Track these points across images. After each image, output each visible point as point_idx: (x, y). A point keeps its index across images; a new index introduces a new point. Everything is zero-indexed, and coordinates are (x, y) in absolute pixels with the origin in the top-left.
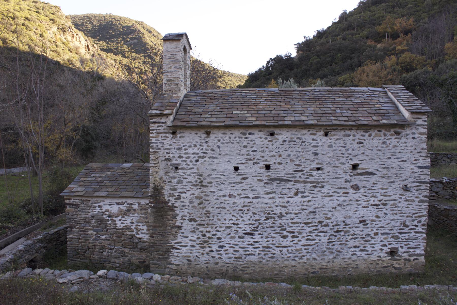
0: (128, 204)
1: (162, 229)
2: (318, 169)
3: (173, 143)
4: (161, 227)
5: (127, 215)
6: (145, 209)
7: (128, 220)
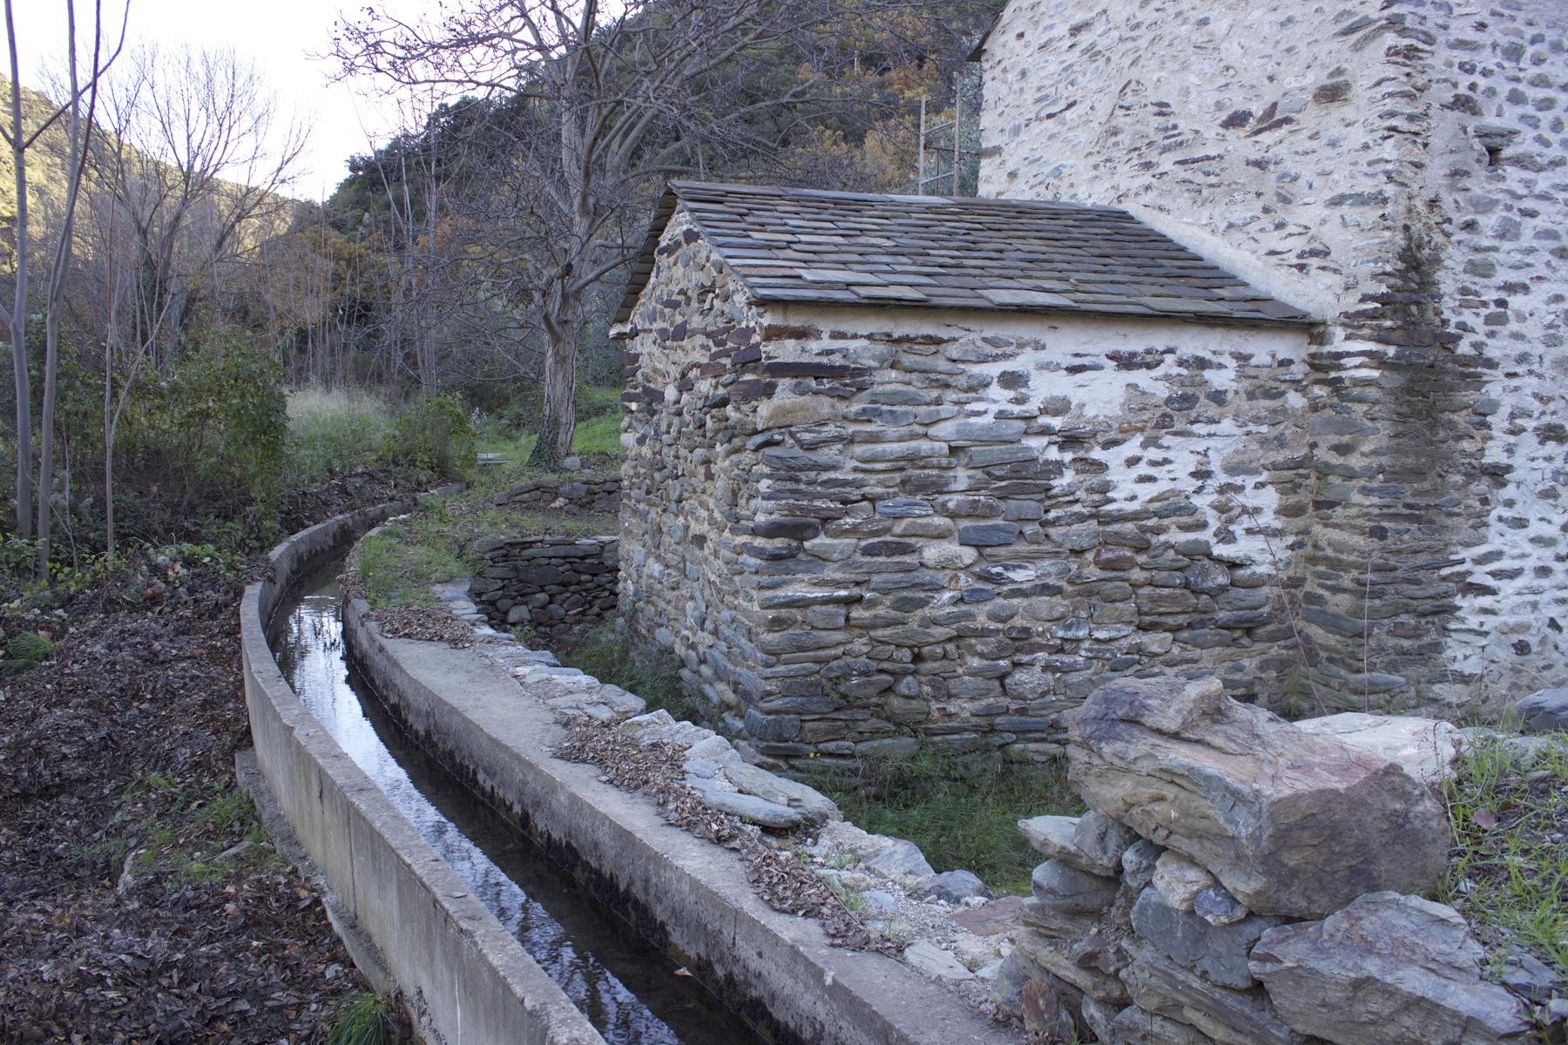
0: (1181, 363)
1: (1426, 485)
3: (1493, 14)
4: (1419, 474)
5: (1178, 427)
6: (1270, 394)
7: (1182, 457)
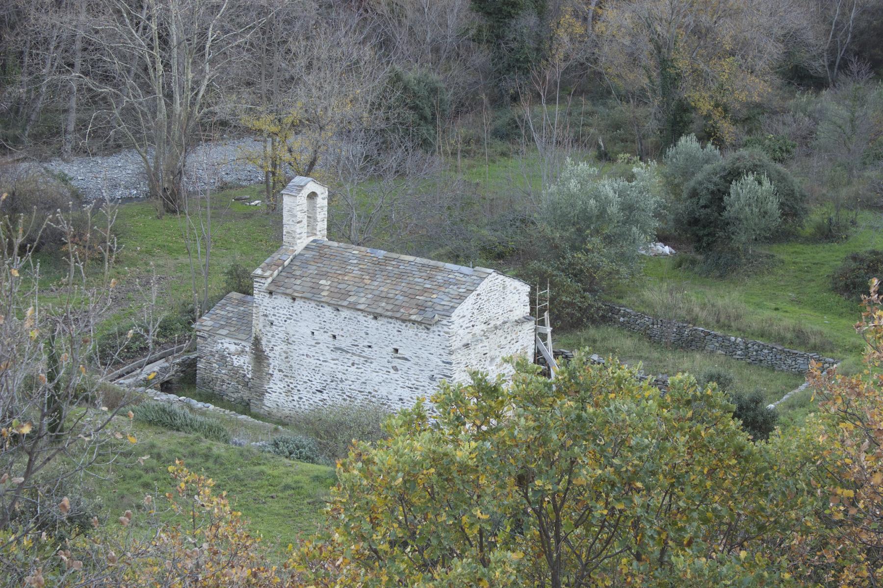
2: (370, 347)
